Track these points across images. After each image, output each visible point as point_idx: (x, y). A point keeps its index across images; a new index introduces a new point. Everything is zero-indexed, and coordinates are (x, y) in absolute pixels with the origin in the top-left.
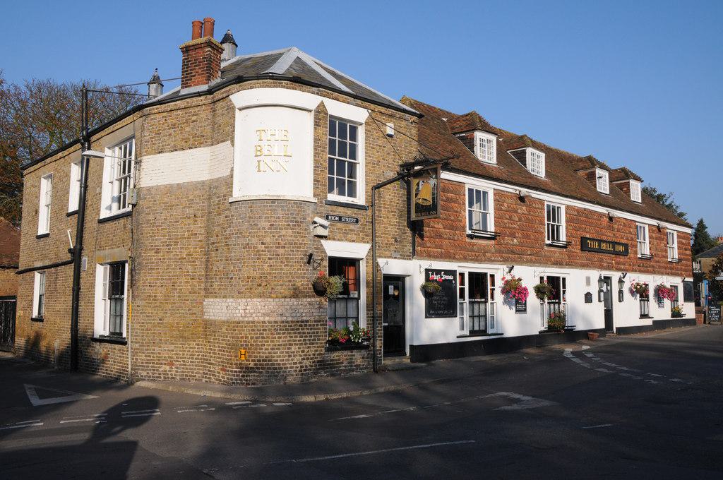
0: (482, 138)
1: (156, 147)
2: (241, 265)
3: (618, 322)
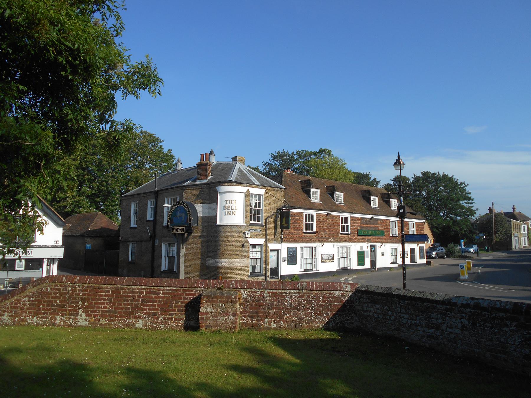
3: (379, 264)
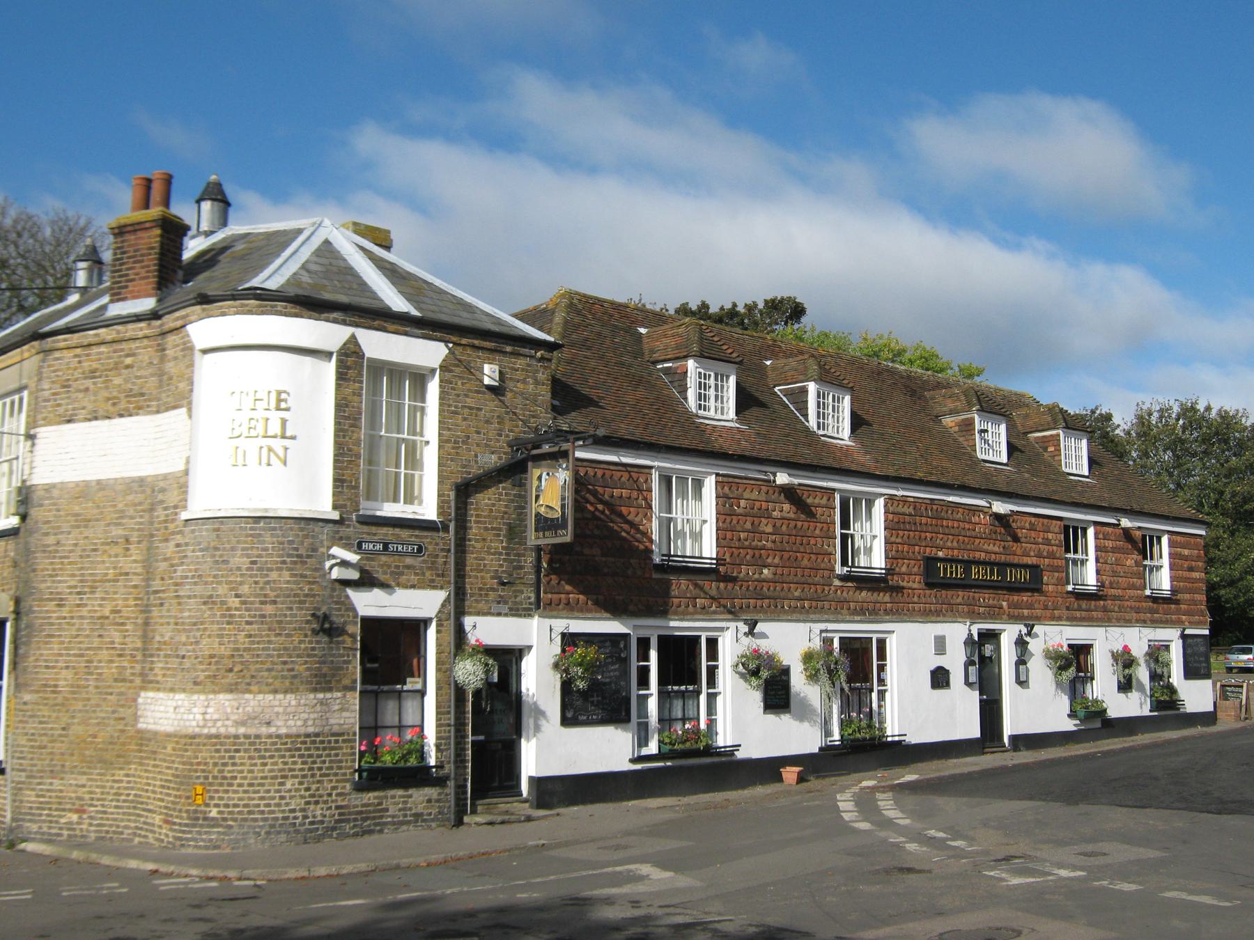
1: (61, 410)
2: (198, 634)
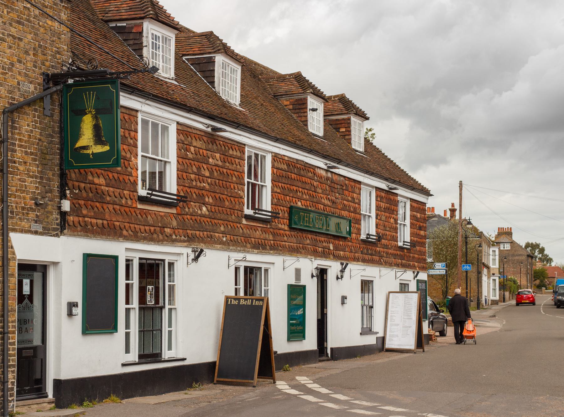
0: (155, 33)
